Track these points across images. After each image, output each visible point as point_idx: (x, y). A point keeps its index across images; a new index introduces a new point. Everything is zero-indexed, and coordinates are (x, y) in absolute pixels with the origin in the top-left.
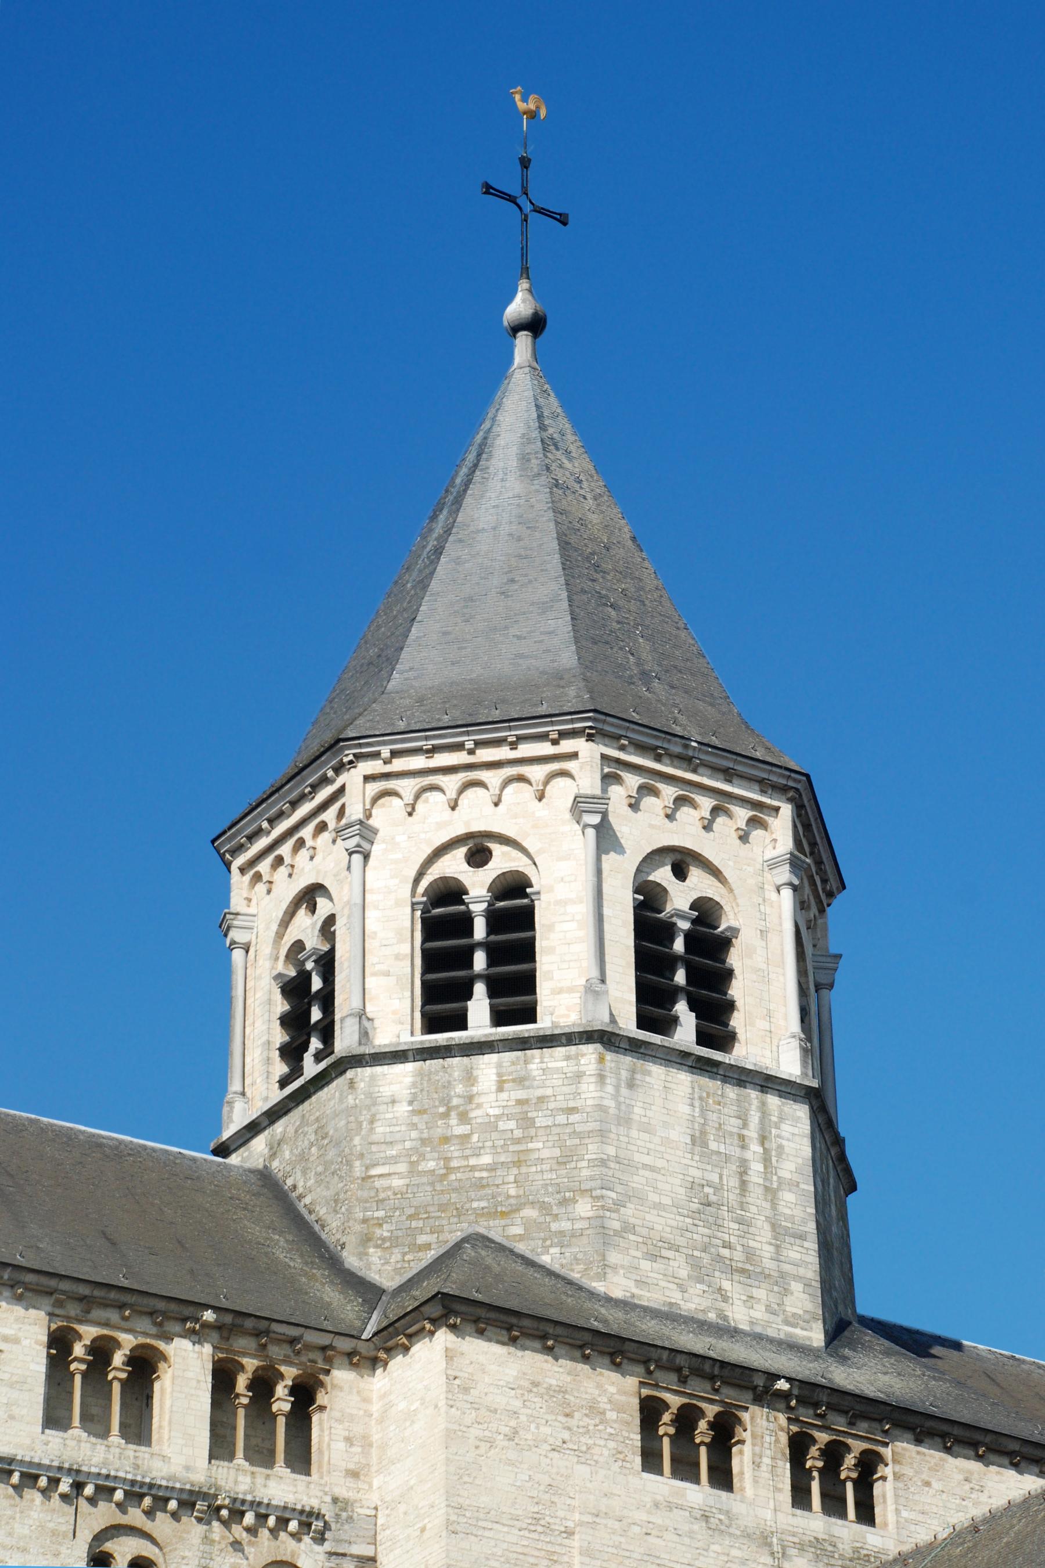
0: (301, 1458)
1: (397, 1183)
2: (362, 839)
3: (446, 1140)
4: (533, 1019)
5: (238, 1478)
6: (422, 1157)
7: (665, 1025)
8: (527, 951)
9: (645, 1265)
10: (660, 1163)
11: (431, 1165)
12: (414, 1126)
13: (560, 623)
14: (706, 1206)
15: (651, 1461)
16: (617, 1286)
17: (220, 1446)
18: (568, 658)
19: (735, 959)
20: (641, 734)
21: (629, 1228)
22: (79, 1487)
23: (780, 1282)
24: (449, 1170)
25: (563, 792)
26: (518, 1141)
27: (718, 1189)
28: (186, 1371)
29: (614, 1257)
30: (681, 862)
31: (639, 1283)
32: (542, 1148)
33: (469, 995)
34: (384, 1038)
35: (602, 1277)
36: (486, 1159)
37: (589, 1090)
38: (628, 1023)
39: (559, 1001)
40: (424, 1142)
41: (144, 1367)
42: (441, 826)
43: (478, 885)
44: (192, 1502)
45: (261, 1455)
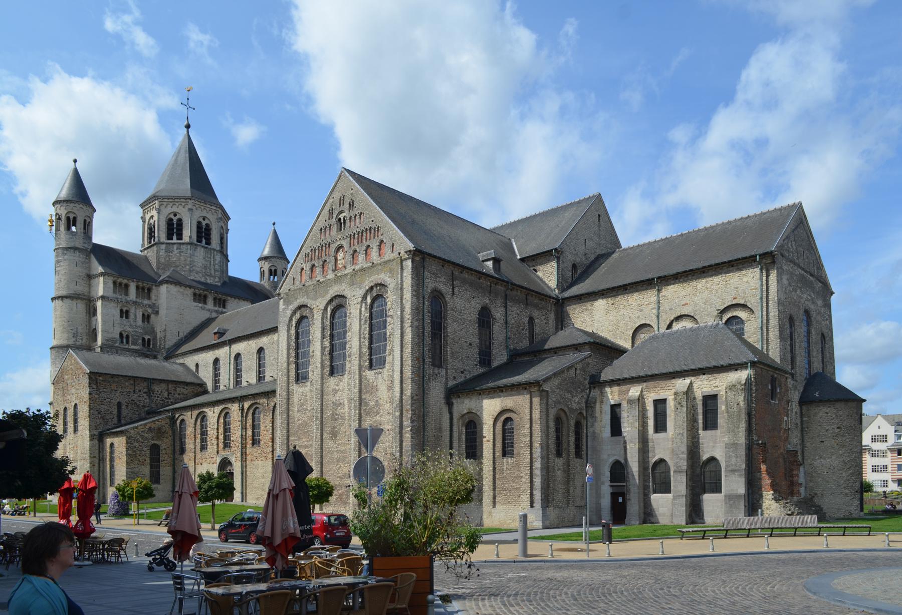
0: (149, 298)
8: (181, 230)
22: (116, 301)
23: (215, 277)
25: (187, 207)
38: (195, 241)
39: (186, 239)
41: (127, 286)
43: (175, 219)
44: (135, 303)
45: (143, 298)
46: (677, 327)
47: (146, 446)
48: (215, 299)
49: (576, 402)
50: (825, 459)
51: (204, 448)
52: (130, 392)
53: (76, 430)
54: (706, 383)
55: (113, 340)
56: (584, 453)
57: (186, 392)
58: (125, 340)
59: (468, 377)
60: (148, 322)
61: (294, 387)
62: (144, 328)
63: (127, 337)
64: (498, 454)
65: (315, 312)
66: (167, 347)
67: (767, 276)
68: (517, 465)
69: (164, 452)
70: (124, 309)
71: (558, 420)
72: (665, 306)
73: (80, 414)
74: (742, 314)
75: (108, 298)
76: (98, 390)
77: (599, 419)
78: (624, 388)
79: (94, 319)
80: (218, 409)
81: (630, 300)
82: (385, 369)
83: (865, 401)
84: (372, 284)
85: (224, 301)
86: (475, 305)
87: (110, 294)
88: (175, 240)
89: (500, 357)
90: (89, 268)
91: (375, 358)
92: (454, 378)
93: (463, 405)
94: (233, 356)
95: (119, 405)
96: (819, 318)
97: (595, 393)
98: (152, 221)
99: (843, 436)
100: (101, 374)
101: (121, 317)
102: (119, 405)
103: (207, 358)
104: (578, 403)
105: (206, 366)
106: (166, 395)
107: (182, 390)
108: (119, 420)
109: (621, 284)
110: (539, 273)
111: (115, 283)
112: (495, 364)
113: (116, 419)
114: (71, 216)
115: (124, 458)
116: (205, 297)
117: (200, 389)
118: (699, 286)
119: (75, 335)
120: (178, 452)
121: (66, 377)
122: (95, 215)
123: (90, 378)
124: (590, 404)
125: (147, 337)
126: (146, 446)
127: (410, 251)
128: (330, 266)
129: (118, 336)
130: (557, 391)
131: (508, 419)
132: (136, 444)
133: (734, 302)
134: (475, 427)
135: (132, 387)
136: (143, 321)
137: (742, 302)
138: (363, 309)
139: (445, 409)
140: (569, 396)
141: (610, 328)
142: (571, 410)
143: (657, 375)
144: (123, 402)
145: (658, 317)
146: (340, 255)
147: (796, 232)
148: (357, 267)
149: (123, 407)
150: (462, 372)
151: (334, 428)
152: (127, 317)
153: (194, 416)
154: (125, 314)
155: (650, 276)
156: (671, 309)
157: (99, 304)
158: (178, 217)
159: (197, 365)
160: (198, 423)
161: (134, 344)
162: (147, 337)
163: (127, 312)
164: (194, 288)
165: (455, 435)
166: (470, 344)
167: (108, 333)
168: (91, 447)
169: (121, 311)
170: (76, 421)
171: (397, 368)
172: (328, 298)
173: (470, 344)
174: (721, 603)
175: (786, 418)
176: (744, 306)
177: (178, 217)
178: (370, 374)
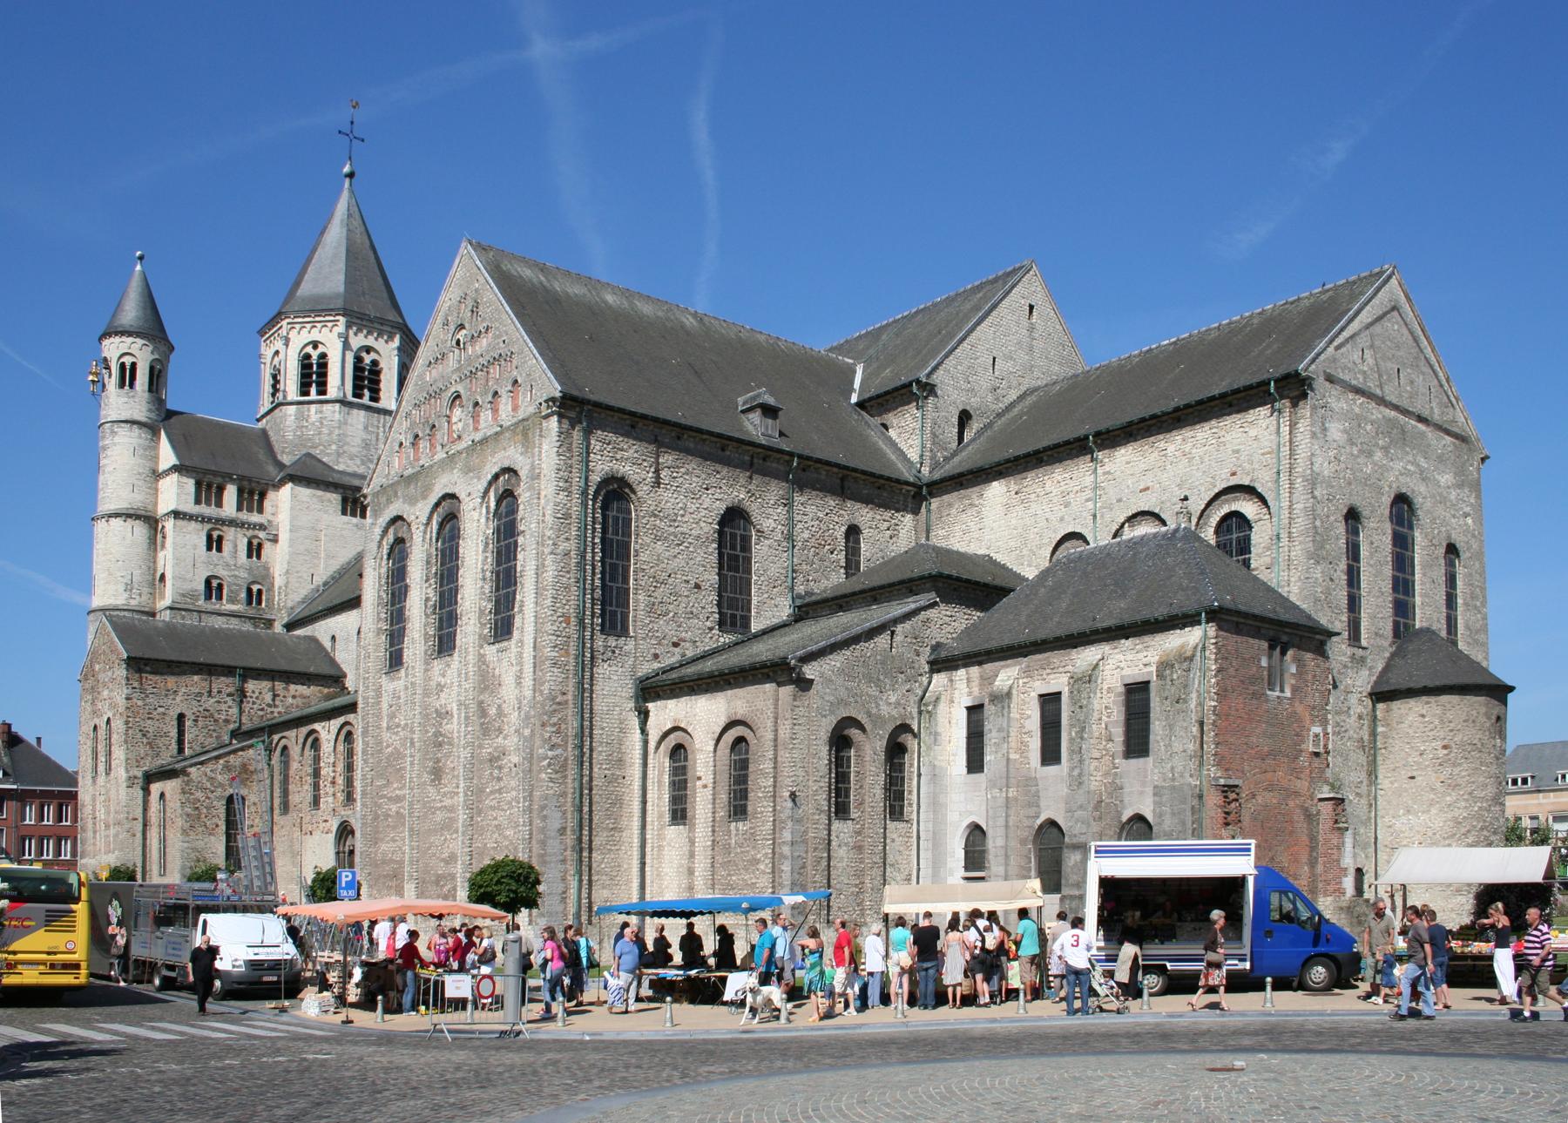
0: (261, 510)
2: (287, 341)
5: (244, 516)
7: (360, 396)
13: (342, 277)
15: (344, 513)
16: (341, 467)
17: (239, 509)
18: (342, 289)
19: (382, 377)
20: (357, 319)
22: (203, 519)
28: (231, 493)
30: (368, 350)
32: (325, 430)
34: (289, 398)
37: (337, 416)
38: (350, 398)
39: (333, 391)
43: (315, 355)
44: (232, 523)
45: (250, 510)
46: (1128, 534)
47: (219, 798)
49: (890, 704)
50: (1416, 814)
51: (316, 802)
52: (200, 694)
54: (1130, 657)
55: (192, 595)
56: (910, 811)
59: (690, 654)
60: (259, 557)
61: (384, 680)
62: (250, 570)
63: (220, 587)
64: (721, 813)
65: (413, 528)
66: (290, 604)
67: (1293, 426)
68: (752, 837)
69: (253, 809)
70: (215, 534)
71: (840, 741)
72: (1111, 493)
74: (1248, 508)
75: (185, 514)
77: (944, 737)
78: (988, 667)
79: (161, 555)
80: (335, 724)
81: (1049, 483)
82: (513, 641)
83: (1511, 689)
84: (496, 469)
86: (714, 505)
88: (313, 395)
89: (769, 606)
90: (155, 459)
91: (502, 628)
92: (656, 656)
93: (664, 713)
95: (181, 717)
96: (1440, 511)
97: (940, 680)
99: (1454, 765)
101: (209, 548)
102: (181, 717)
104: (898, 704)
105: (347, 640)
106: (268, 698)
108: (181, 750)
109: (1030, 449)
110: (892, 433)
112: (755, 627)
113: (174, 746)
114: (128, 360)
115: (180, 822)
118: (1171, 448)
119: (129, 587)
120: (277, 812)
122: (172, 357)
124: (926, 708)
125: (255, 588)
126: (219, 798)
127: (553, 399)
128: (442, 436)
129: (202, 587)
130: (839, 681)
131: (740, 740)
132: (199, 795)
133: (1234, 481)
134: (686, 759)
135: (206, 684)
136: (250, 556)
137: (1246, 482)
138: (483, 520)
139: (634, 722)
140: (873, 691)
141: (1012, 544)
142: (878, 720)
143: (1044, 642)
144: (189, 714)
145: (1095, 516)
146: (457, 413)
147: (1377, 328)
148: (478, 436)
150: (676, 645)
151: (438, 761)
152: (219, 549)
153: (334, 730)
154: (214, 543)
155: (1081, 432)
156: (1119, 500)
157: (169, 524)
158: (321, 349)
159: (333, 638)
160: (341, 748)
161: (232, 601)
163: (220, 539)
165: (652, 774)
166: (697, 586)
167: (185, 580)
169: (209, 537)
171: (529, 640)
172: (433, 499)
173: (697, 586)
174: (365, 1109)
175: (1317, 729)
176: (1249, 491)
177: (321, 349)
178: (490, 651)
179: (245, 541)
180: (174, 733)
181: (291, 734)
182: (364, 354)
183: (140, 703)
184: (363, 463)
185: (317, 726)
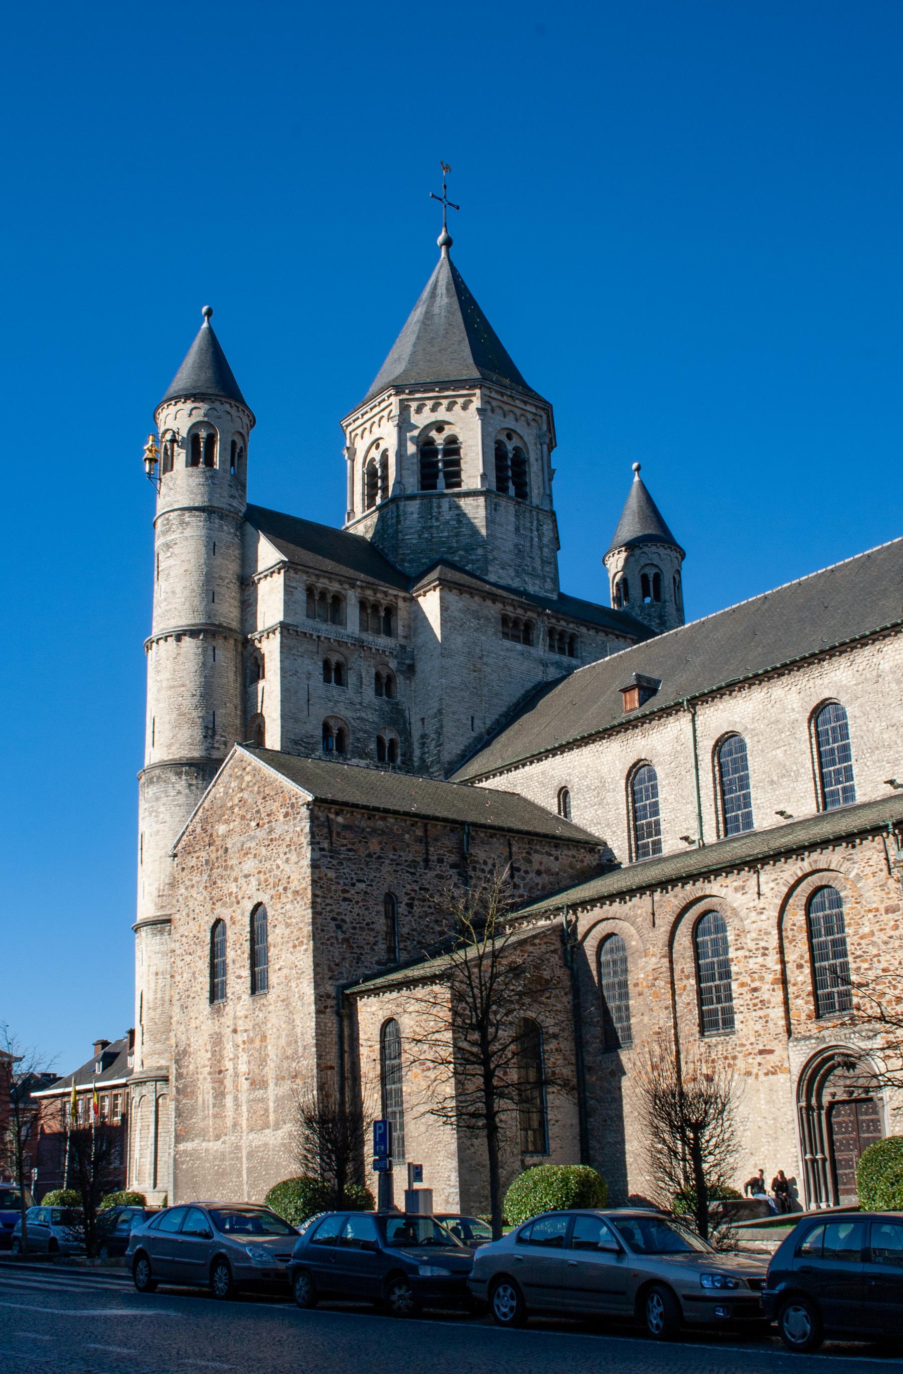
1: (414, 541)
3: (431, 527)
4: (460, 486)
6: (423, 533)
9: (501, 571)
10: (505, 537)
11: (426, 535)
12: (419, 522)
14: (519, 552)
17: (364, 627)
21: (495, 559)
24: (433, 537)
26: (456, 528)
27: (524, 546)
29: (490, 568)
31: (499, 577)
33: (437, 477)
35: (486, 575)
36: (446, 534)
40: (423, 528)
42: (426, 418)
45: (377, 632)
48: (551, 632)
53: (258, 984)
57: (555, 867)
58: (333, 744)
63: (341, 734)
67: (342, 1103)
70: (334, 658)
73: (275, 935)
76: (333, 852)
85: (573, 638)
87: (300, 618)
94: (707, 745)
98: (376, 454)
100: (342, 806)
101: (327, 680)
102: (390, 900)
103: (609, 760)
107: (546, 859)
111: (310, 590)
113: (382, 946)
116: (529, 627)
117: (590, 860)
121: (222, 829)
123: (313, 818)
125: (388, 736)
129: (319, 732)
136: (378, 693)
149: (402, 909)
152: (340, 681)
154: (335, 673)
162: (388, 736)
163: (339, 667)
164: (503, 601)
168: (321, 1033)
169: (326, 663)
170: (257, 957)
179: (373, 671)
180: (381, 923)
181: (640, 905)
182: (433, 434)
183: (331, 874)
184: (518, 574)
185: (717, 887)
